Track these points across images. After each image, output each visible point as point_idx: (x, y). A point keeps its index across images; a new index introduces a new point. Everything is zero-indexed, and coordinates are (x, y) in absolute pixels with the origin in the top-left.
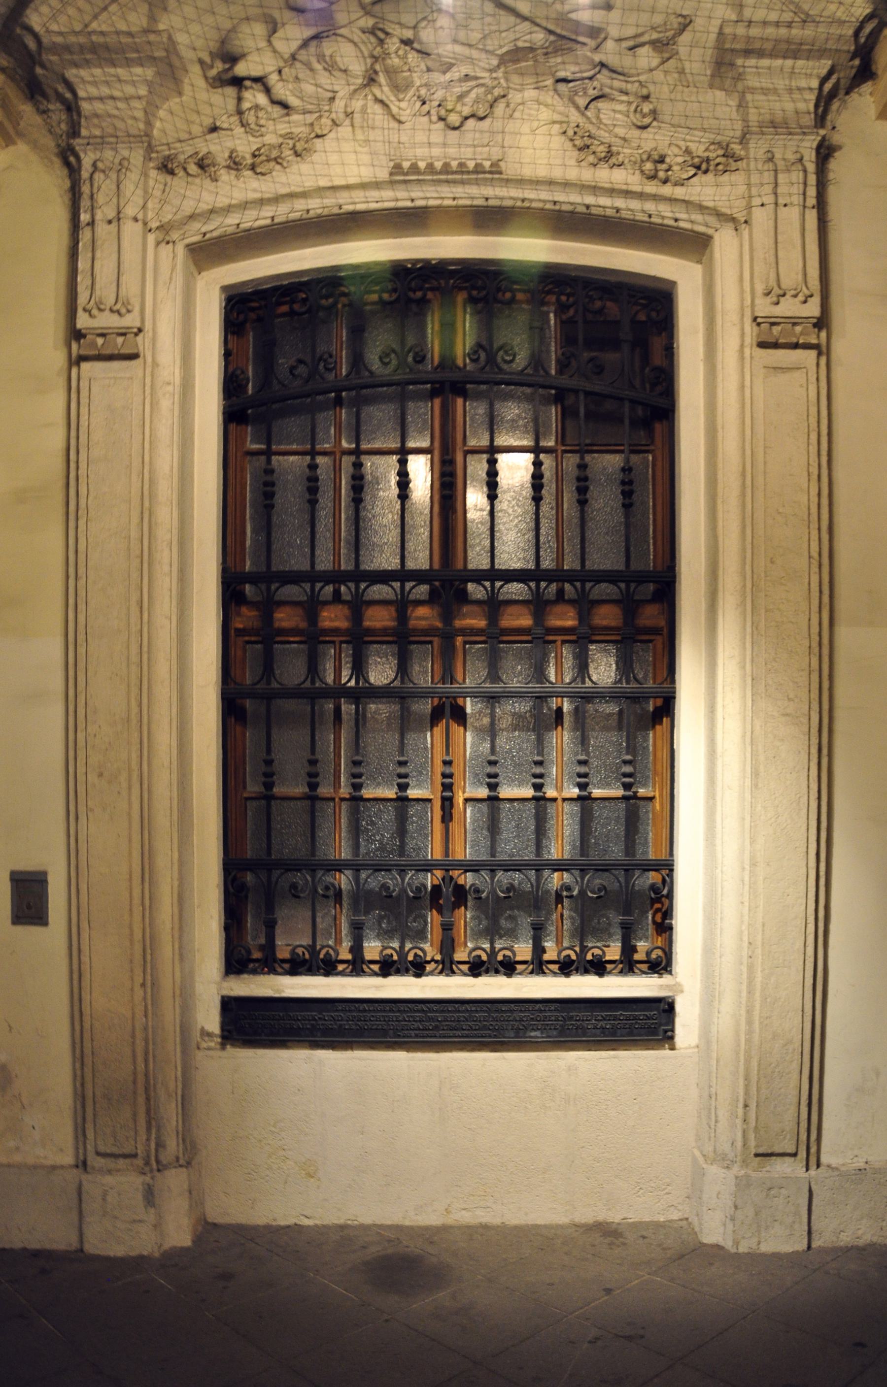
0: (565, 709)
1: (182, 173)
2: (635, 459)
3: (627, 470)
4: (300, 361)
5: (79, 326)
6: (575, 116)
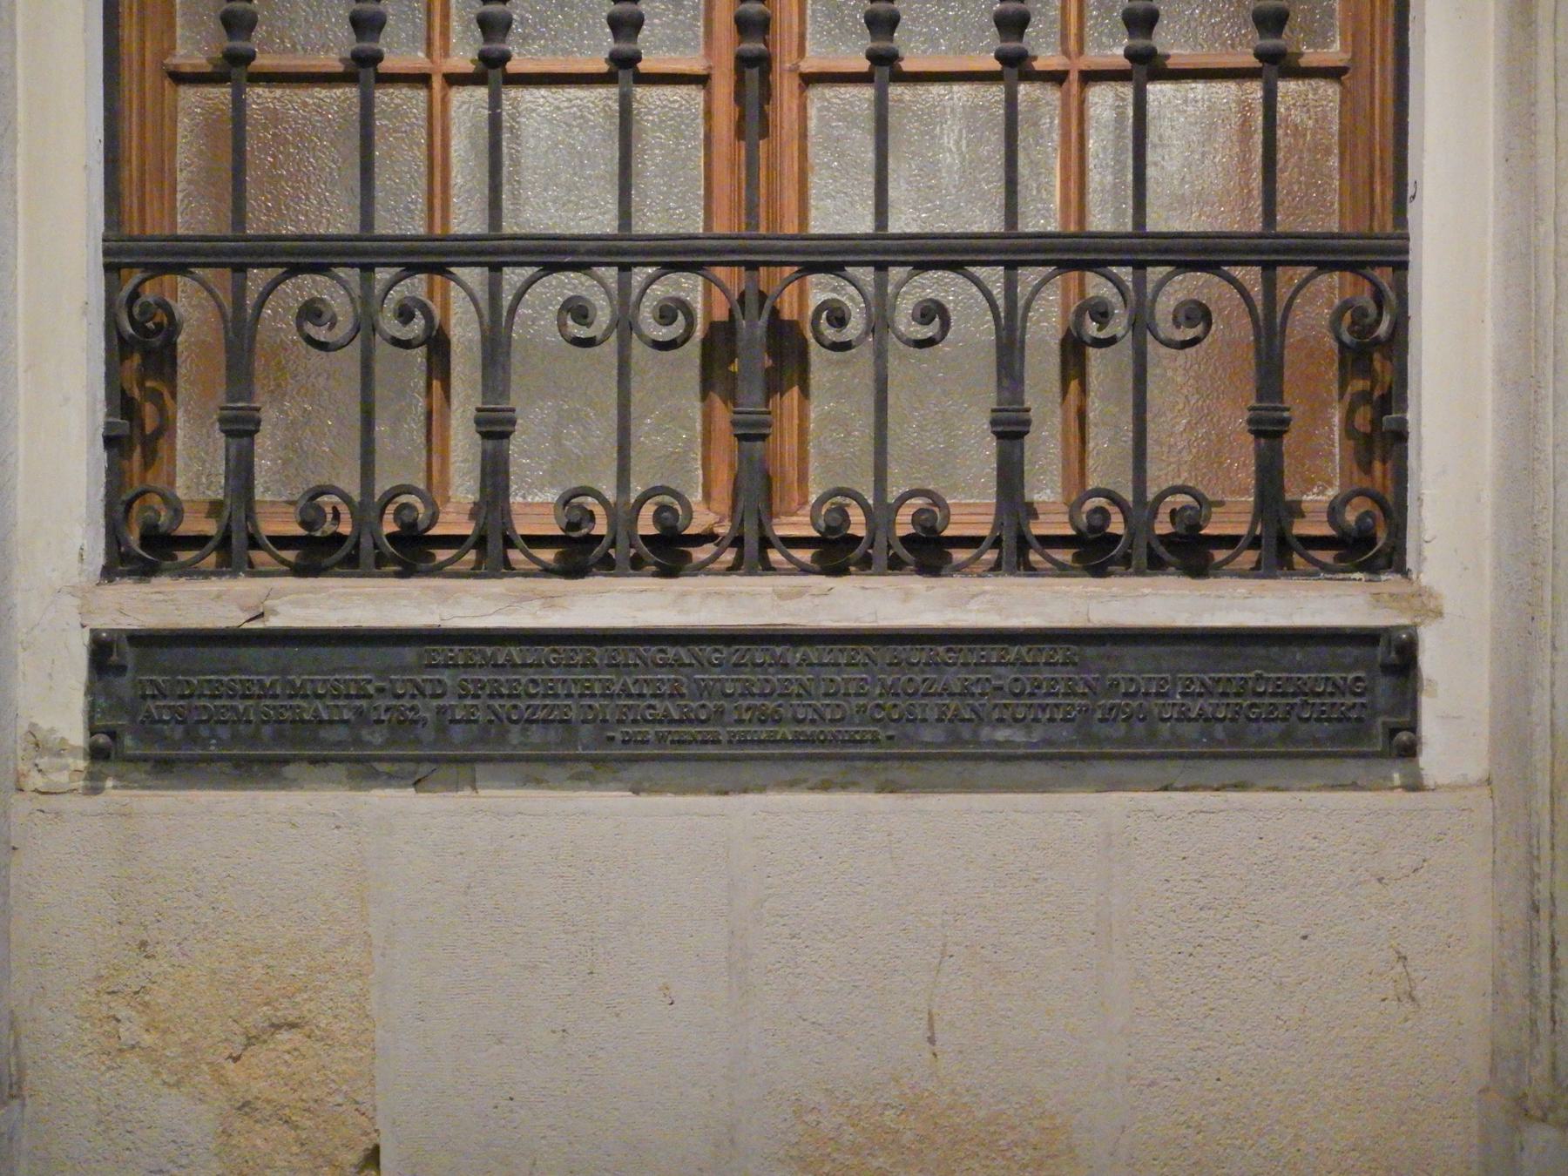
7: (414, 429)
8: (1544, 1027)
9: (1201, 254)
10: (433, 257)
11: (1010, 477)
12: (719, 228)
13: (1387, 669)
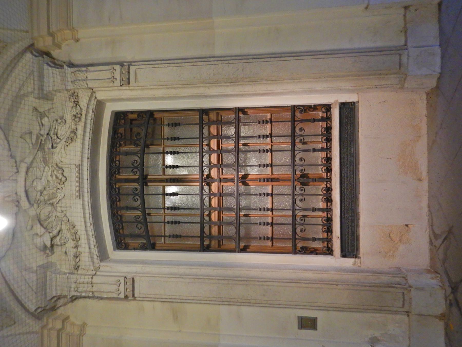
0: (243, 143)
1: (79, 263)
2: (166, 123)
3: (169, 125)
4: (137, 226)
5: (123, 297)
6: (63, 142)
7: (313, 219)
8: (392, 86)
9: (294, 129)
10: (294, 216)
11: (319, 150)
12: (291, 184)
13: (344, 106)
